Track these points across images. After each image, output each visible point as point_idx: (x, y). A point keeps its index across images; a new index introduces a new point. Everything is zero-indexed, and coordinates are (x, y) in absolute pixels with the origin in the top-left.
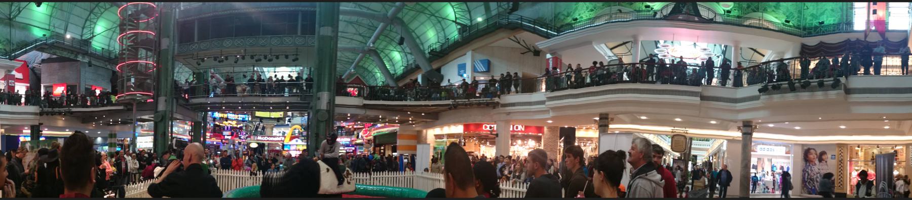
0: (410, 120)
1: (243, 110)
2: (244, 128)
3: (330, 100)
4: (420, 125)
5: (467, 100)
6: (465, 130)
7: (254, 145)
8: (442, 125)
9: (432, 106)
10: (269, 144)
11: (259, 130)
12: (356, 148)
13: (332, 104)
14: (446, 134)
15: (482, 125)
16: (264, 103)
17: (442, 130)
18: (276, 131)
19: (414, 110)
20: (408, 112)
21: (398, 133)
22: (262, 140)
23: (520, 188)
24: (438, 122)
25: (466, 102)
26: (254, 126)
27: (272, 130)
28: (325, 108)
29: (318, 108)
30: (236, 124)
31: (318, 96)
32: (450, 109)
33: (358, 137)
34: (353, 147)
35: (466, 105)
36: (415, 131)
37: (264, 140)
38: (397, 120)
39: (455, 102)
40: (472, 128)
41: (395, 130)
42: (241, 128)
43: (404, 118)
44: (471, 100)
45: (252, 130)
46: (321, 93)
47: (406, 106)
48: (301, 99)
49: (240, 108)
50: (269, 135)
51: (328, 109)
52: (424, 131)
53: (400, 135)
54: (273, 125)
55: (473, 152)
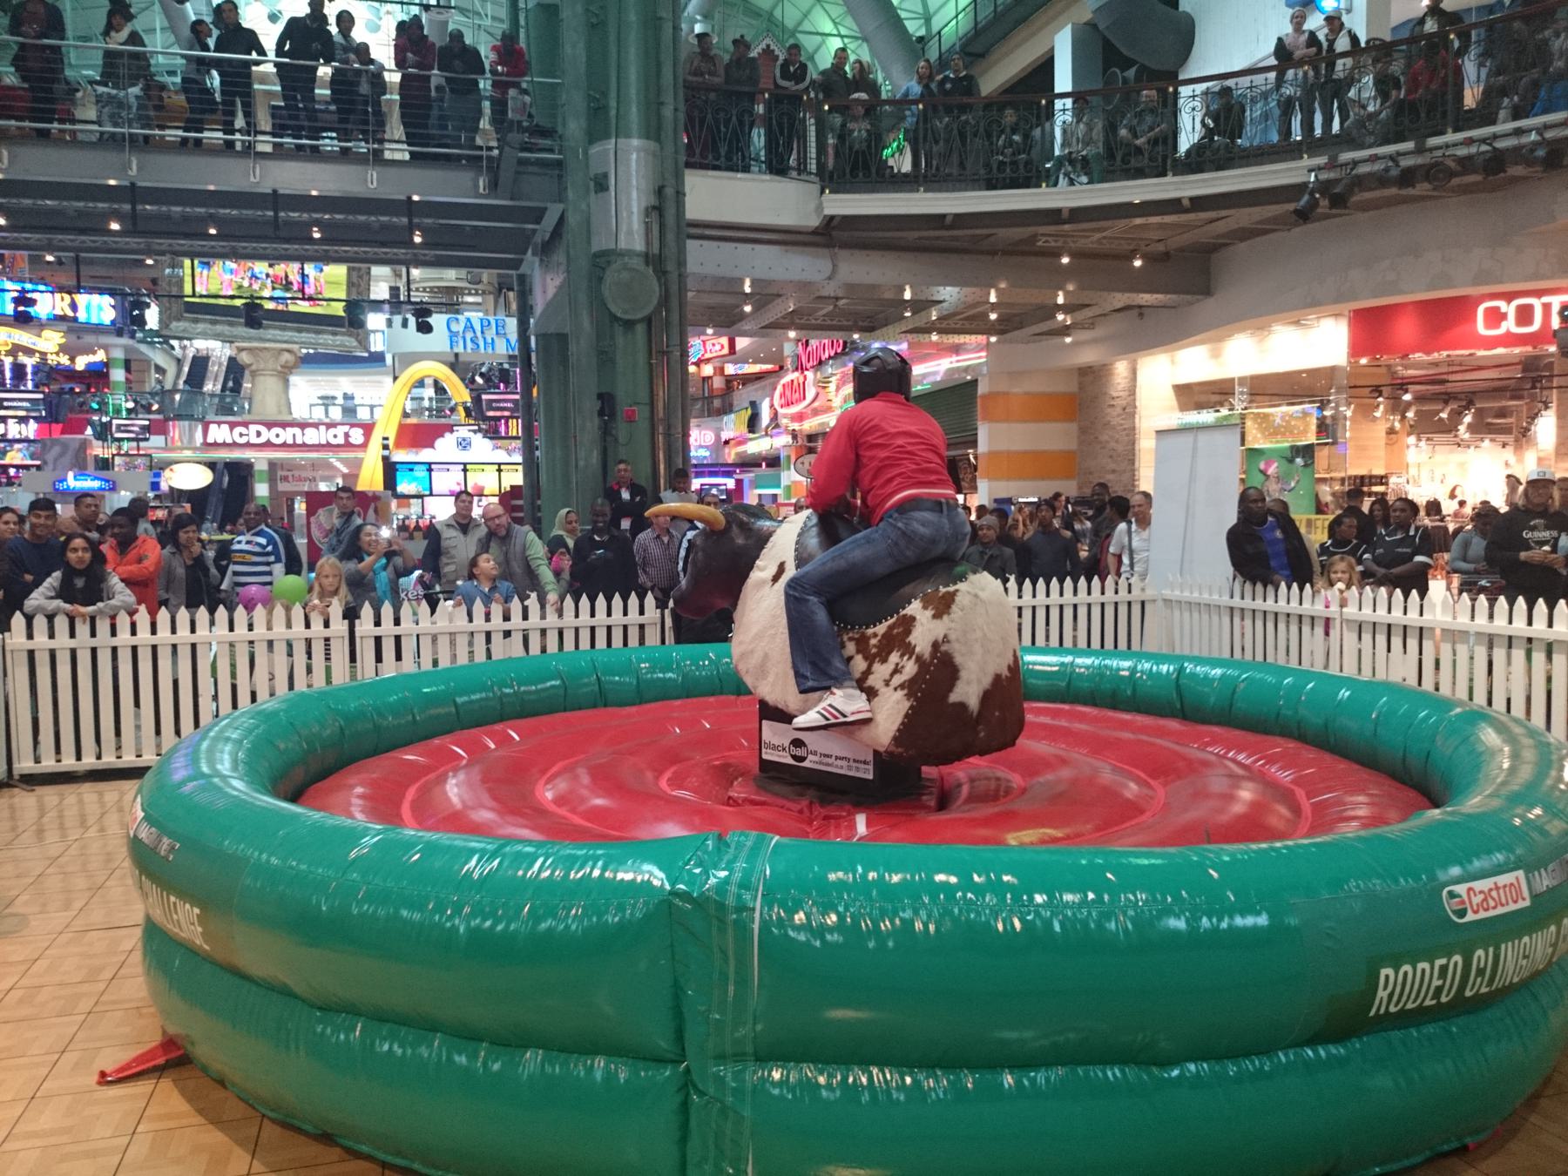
0: (1059, 308)
1: (133, 242)
2: (118, 375)
3: (660, 192)
4: (1098, 332)
5: (1409, 145)
6: (1356, 350)
7: (192, 477)
8: (1216, 327)
9: (1198, 203)
10: (273, 465)
11: (208, 387)
12: (739, 483)
13: (670, 219)
14: (1242, 381)
15: (1475, 302)
16: (276, 200)
17: (1216, 355)
18: (305, 393)
19: (1093, 237)
20: (1059, 256)
21: (982, 389)
22: (235, 445)
23: (1243, 598)
24: (1209, 304)
25: (1406, 162)
26: (179, 362)
27: (286, 383)
28: (639, 246)
29: (600, 243)
30: (63, 349)
31: (595, 169)
32: (1304, 216)
33: (753, 424)
34: (728, 474)
35: (1407, 177)
36: (1068, 371)
37: (248, 445)
38: (994, 307)
39: (1332, 165)
40: (1406, 329)
41: (966, 369)
42: (97, 377)
43: (1030, 296)
44: (1433, 141)
45: (168, 386)
46: (610, 144)
47: (1053, 216)
48: (494, 185)
49: (115, 226)
50: (272, 413)
51: (656, 249)
52: (1121, 368)
53: (988, 397)
54: (286, 357)
55: (1382, 480)
